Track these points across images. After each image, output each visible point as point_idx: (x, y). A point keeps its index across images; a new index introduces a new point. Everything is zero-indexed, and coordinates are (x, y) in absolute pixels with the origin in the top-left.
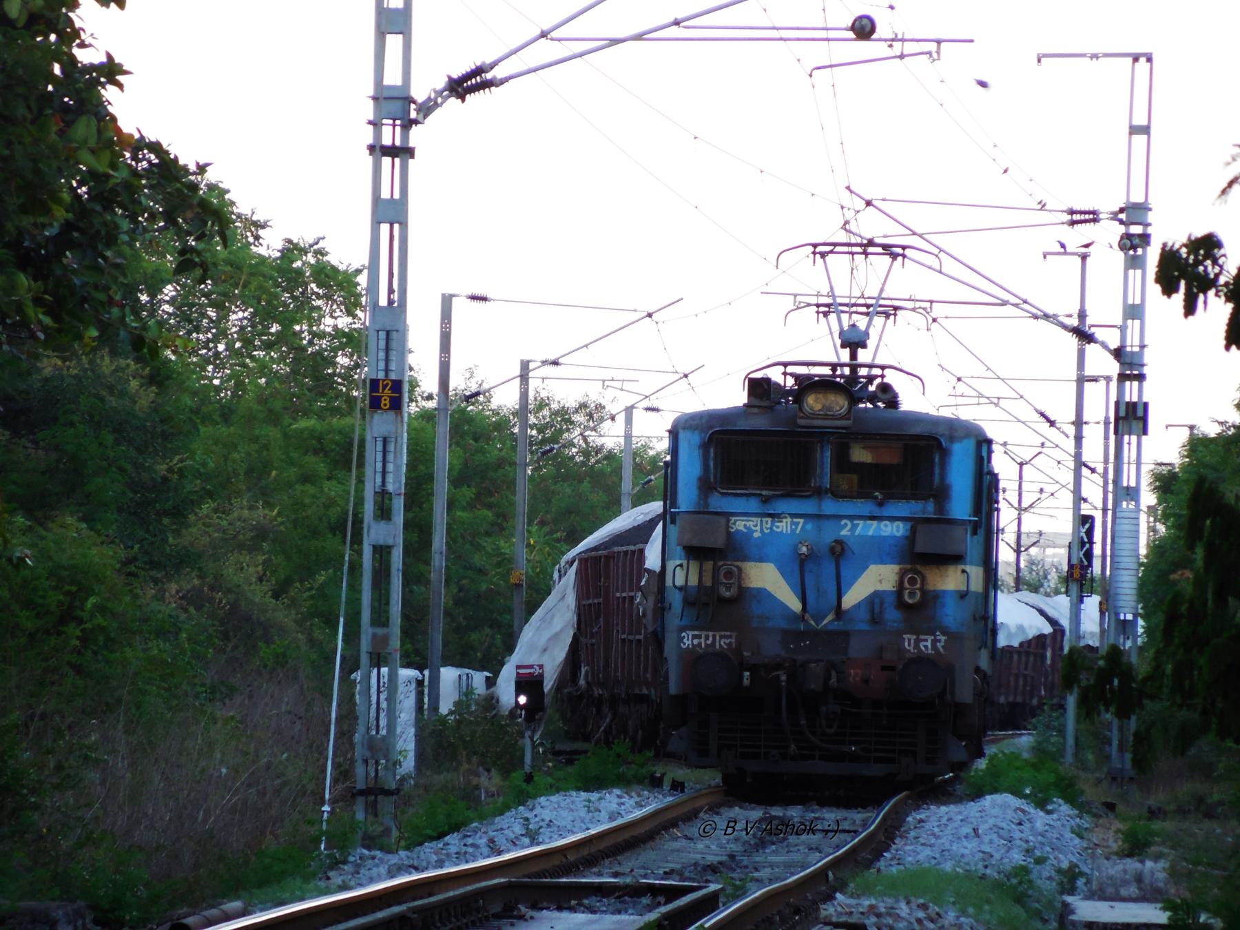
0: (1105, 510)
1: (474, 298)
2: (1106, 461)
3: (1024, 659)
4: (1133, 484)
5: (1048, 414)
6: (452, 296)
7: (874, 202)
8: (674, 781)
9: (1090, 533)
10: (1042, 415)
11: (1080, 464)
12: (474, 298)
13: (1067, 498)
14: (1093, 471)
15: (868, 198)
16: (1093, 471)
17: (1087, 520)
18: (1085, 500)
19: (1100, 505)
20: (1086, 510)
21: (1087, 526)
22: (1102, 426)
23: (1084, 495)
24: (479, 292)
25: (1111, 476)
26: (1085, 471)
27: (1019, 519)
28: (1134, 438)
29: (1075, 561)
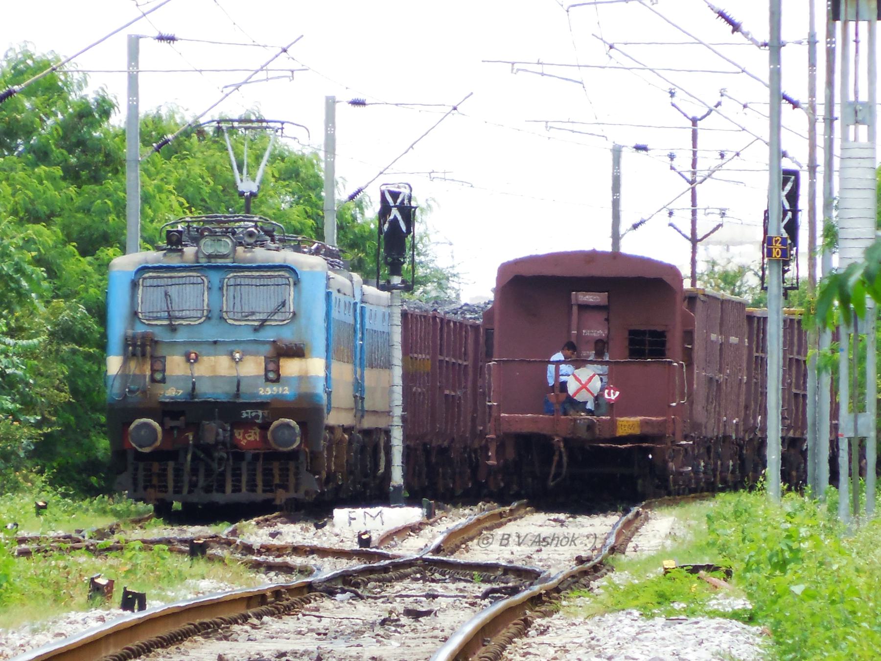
0: (812, 168)
1: (161, 38)
2: (812, 93)
3: (853, 163)
4: (863, 97)
5: (729, 13)
6: (138, 38)
7: (615, 46)
8: (126, 593)
9: (793, 197)
10: (722, 15)
11: (778, 97)
12: (161, 38)
13: (763, 153)
14: (795, 105)
15: (610, 42)
16: (795, 105)
17: (790, 177)
18: (784, 155)
19: (805, 161)
20: (787, 164)
21: (788, 187)
22: (805, 48)
23: (784, 148)
24: (166, 32)
25: (821, 111)
26: (786, 107)
27: (705, 179)
28: (863, 26)
29: (772, 233)
